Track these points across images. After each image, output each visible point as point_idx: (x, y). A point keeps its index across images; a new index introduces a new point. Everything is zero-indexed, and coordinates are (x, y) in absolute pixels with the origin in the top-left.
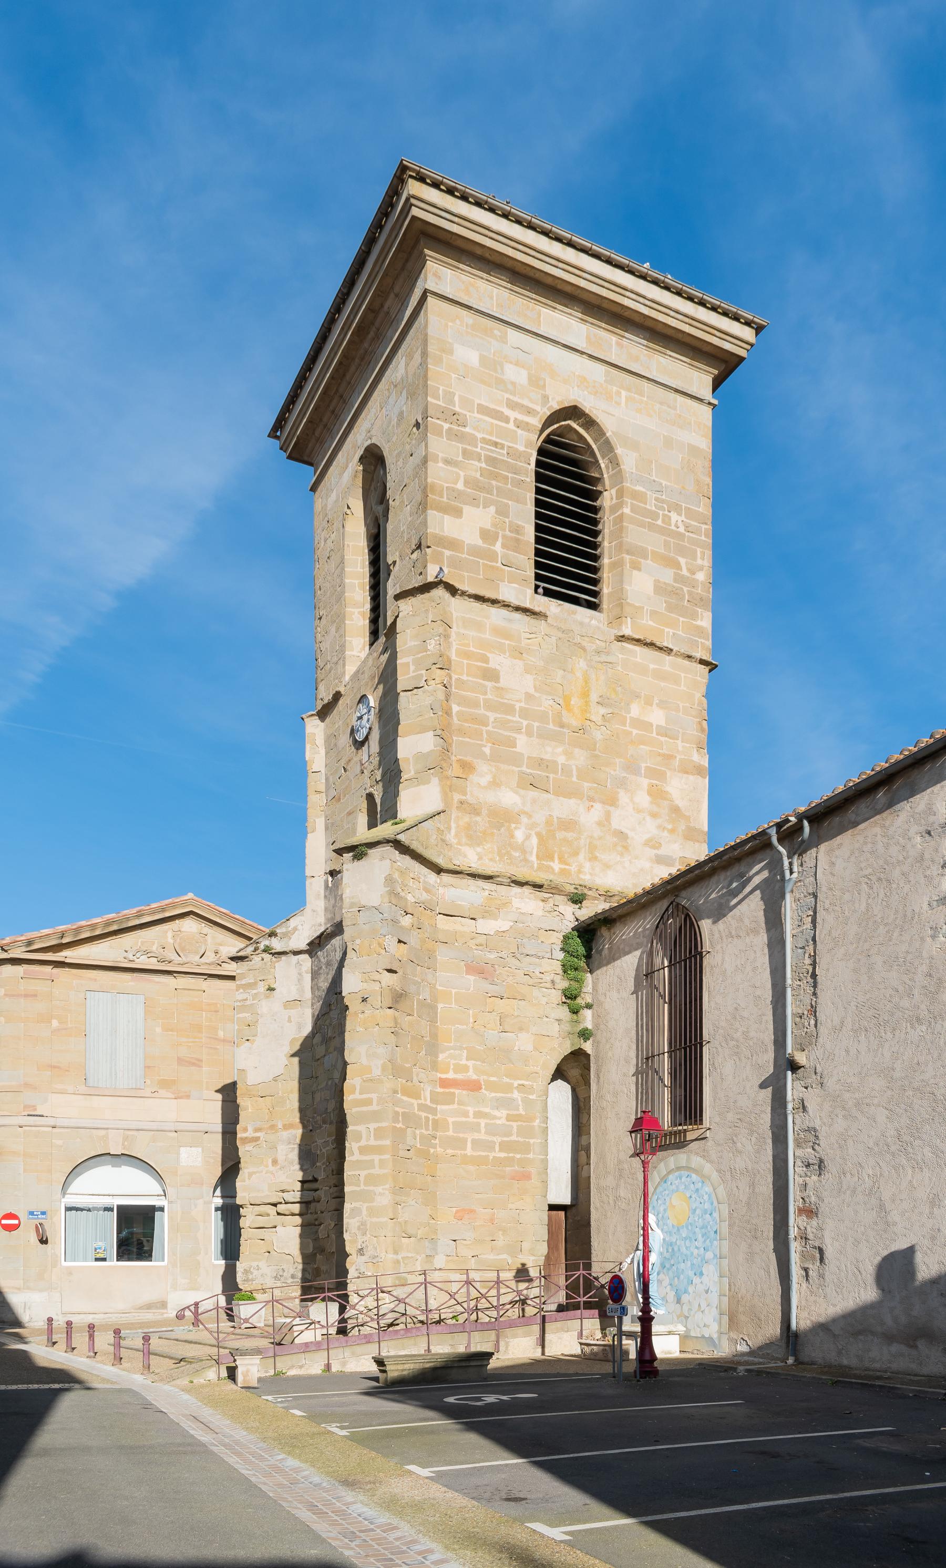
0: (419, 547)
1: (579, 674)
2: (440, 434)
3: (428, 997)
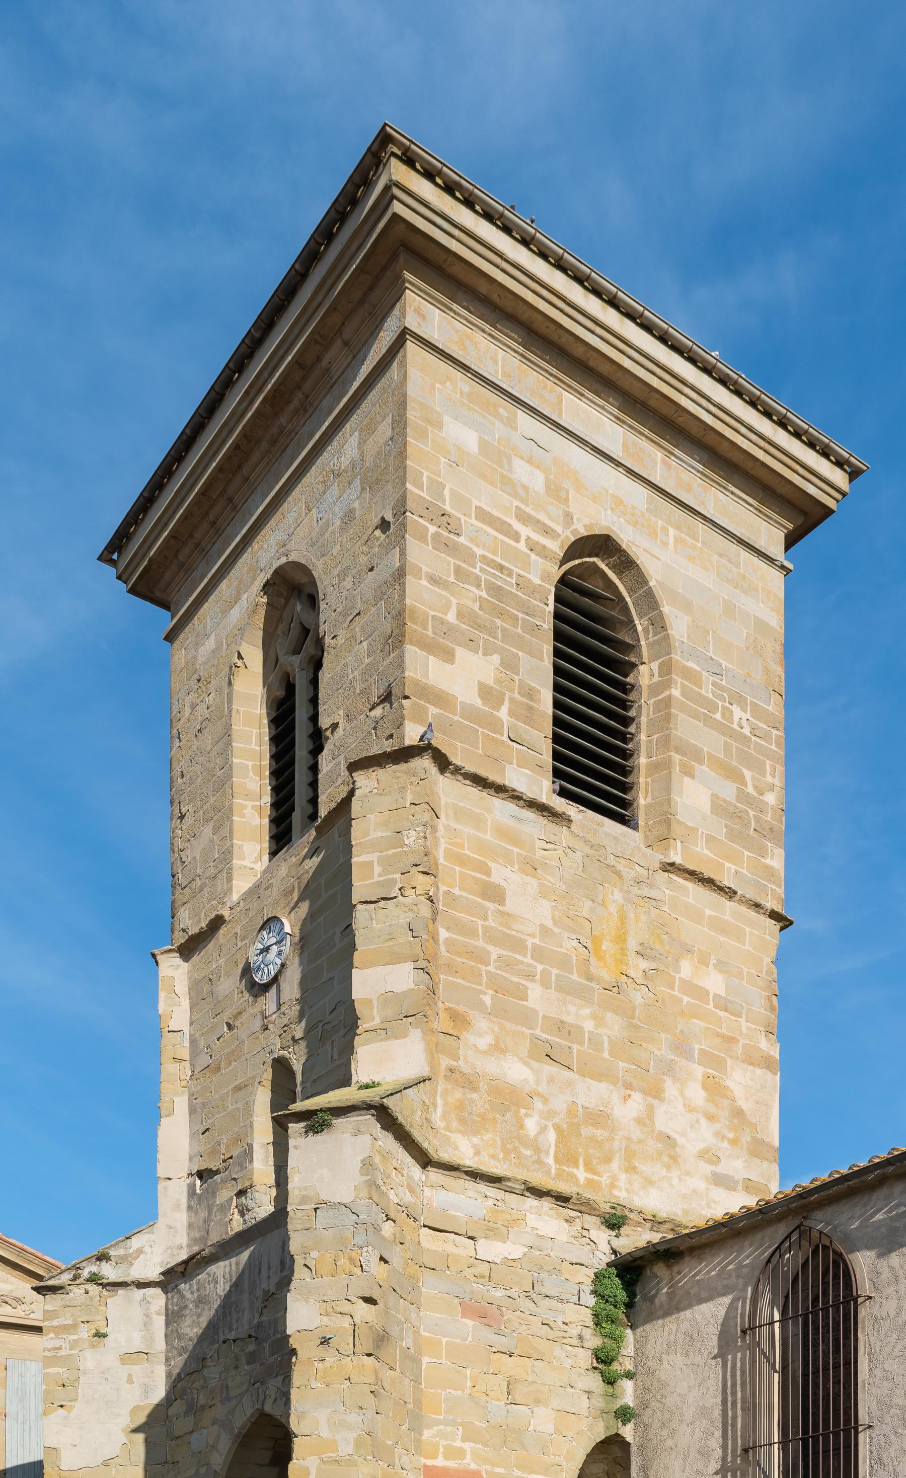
0: (387, 698)
1: (612, 909)
2: (423, 538)
3: (411, 1346)
